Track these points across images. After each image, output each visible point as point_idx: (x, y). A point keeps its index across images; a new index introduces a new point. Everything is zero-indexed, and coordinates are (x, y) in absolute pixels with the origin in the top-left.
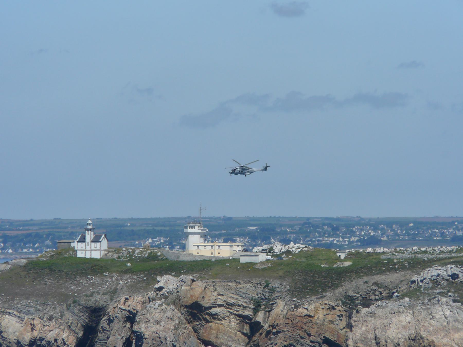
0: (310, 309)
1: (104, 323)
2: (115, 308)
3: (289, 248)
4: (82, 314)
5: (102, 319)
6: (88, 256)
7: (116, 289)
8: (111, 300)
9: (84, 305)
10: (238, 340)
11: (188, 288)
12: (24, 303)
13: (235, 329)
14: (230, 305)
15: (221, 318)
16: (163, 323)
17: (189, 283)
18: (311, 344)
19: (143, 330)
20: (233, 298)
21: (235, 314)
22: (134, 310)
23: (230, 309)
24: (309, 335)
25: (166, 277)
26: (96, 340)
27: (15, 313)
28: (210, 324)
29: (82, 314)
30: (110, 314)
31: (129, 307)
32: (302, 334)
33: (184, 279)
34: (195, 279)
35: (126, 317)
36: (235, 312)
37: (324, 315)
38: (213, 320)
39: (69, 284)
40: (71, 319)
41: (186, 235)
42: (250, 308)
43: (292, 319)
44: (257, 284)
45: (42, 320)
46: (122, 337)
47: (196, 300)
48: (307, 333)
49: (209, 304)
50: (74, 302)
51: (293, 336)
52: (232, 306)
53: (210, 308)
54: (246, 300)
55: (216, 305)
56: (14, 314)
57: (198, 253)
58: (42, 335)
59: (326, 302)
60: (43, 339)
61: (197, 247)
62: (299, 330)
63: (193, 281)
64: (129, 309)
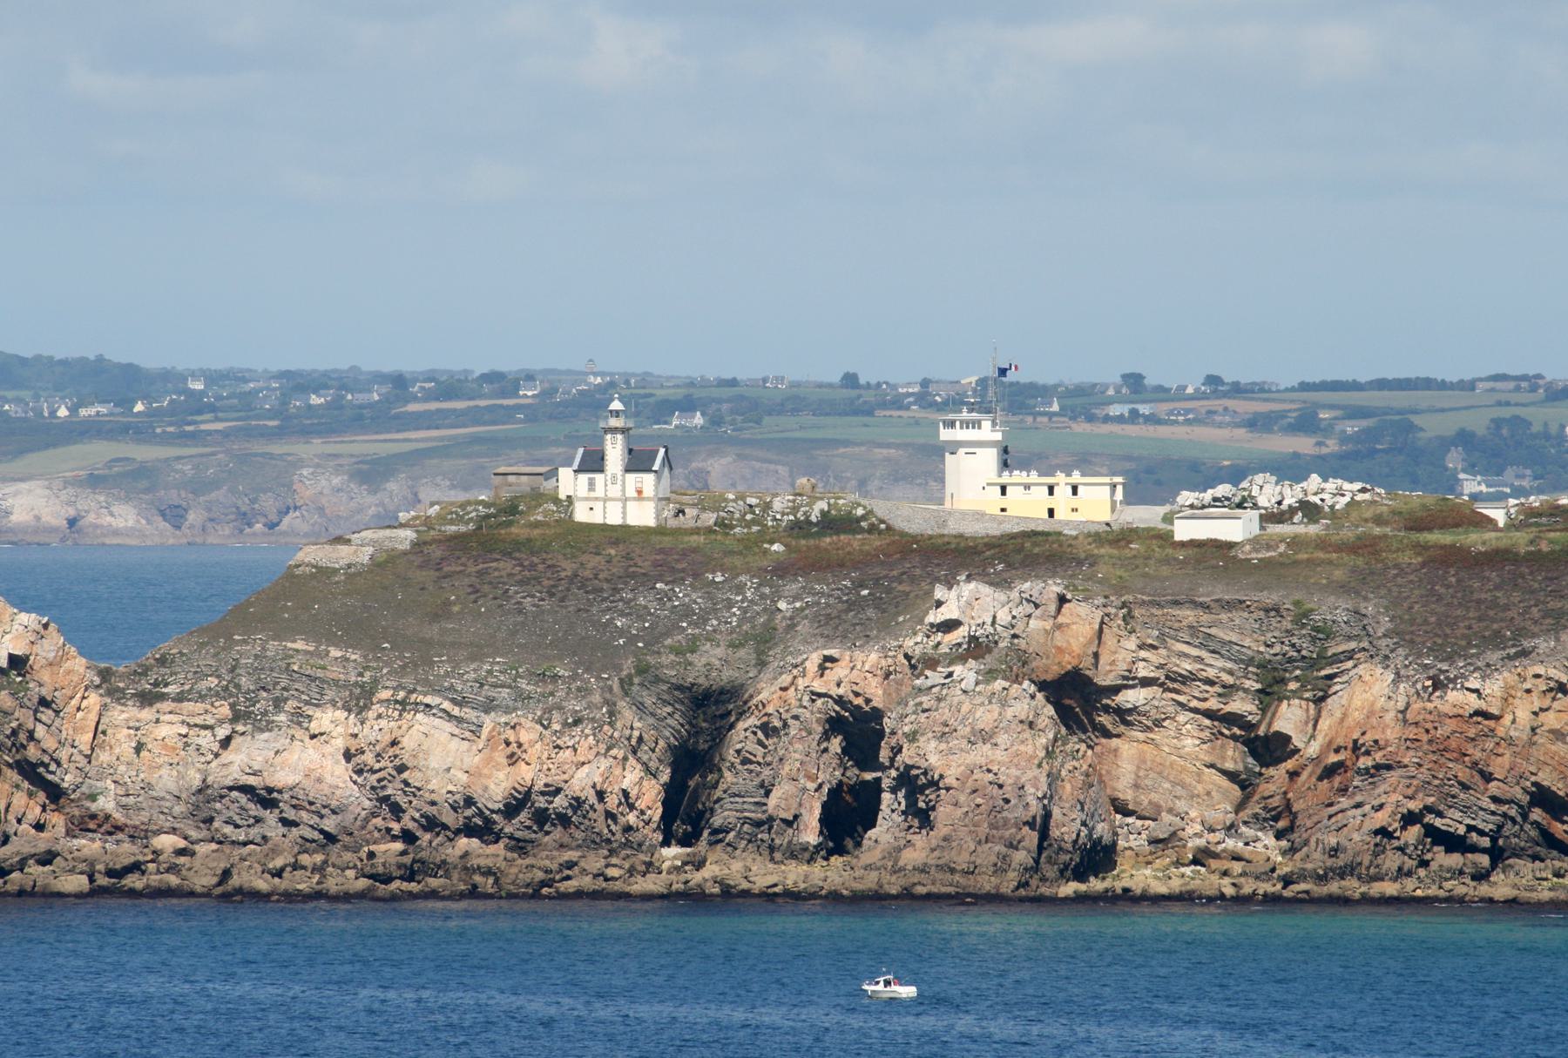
0: (1488, 691)
1: (742, 735)
2: (784, 689)
3: (1305, 492)
4: (669, 709)
5: (732, 726)
6: (614, 519)
7: (770, 629)
8: (762, 664)
9: (674, 680)
10: (1208, 794)
11: (1048, 625)
12: (473, 675)
13: (1197, 759)
14: (1173, 681)
15: (1149, 723)
16: (1002, 739)
17: (1053, 608)
18: (1493, 807)
19: (933, 759)
20: (1187, 656)
21: (1195, 711)
22: (857, 694)
23: (1177, 692)
24: (1488, 778)
25: (968, 589)
26: (718, 793)
27: (446, 705)
28: (1115, 742)
29: (669, 709)
30: (770, 709)
31: (838, 685)
32: (1464, 774)
33: (1035, 593)
34: (1069, 596)
35: (830, 720)
36: (1194, 704)
37: (1535, 714)
38: (1122, 728)
39: (604, 612)
40: (637, 724)
41: (941, 450)
42: (1246, 691)
43: (1429, 726)
44: (1267, 611)
45: (545, 728)
46: (820, 786)
47: (1075, 662)
48: (1481, 772)
49: (1111, 676)
50: (642, 670)
51: (1436, 782)
52: (1184, 683)
53: (1116, 690)
54: (1229, 665)
55: (1130, 681)
56: (444, 711)
57: (1003, 510)
58: (556, 779)
59: (1540, 670)
60: (558, 791)
61: (977, 486)
62: (1456, 760)
63: (1062, 600)
64: (841, 691)
